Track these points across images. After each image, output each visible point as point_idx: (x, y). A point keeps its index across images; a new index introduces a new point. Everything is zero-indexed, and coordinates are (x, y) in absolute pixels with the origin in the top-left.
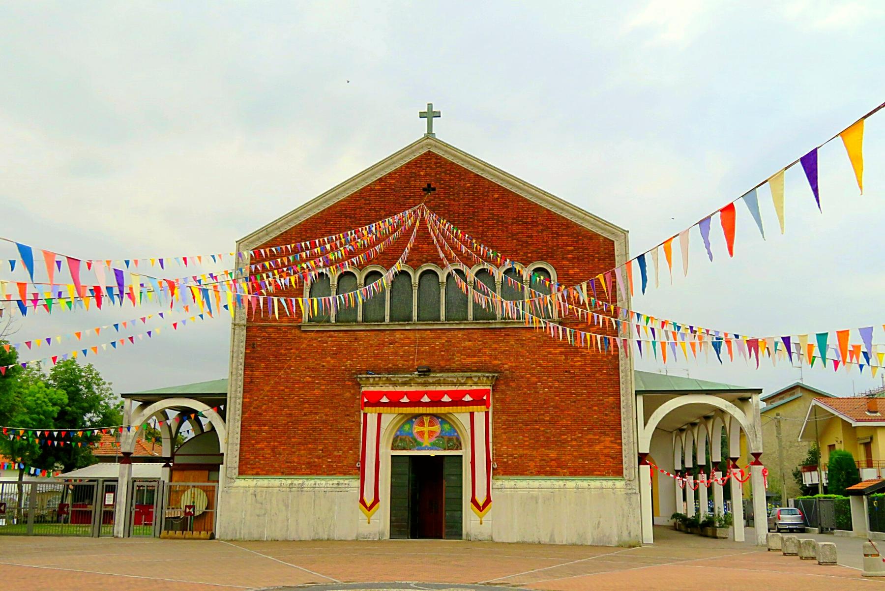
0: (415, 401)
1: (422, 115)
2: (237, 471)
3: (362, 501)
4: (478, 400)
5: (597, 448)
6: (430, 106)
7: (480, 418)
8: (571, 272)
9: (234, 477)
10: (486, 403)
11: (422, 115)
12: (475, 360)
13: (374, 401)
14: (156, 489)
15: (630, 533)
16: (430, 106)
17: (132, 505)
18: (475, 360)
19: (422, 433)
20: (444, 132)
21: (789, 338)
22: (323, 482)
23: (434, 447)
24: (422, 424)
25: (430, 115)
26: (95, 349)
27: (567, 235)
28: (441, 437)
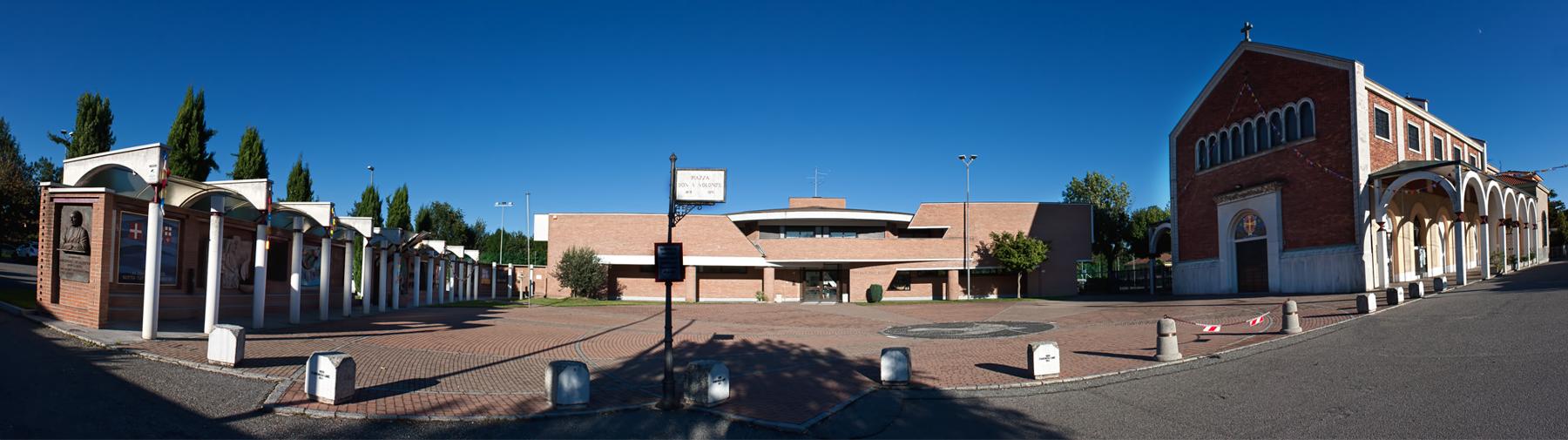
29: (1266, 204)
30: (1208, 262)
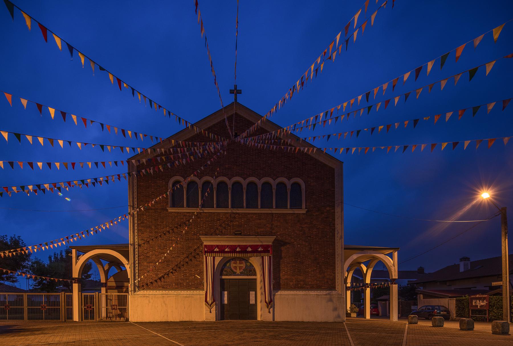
0: (233, 249)
1: (232, 92)
3: (206, 301)
4: (266, 249)
6: (236, 87)
7: (266, 259)
10: (268, 252)
11: (232, 92)
13: (210, 250)
14: (83, 319)
16: (236, 87)
17: (82, 305)
19: (236, 268)
20: (241, 99)
21: (230, 90)
23: (242, 274)
24: (236, 263)
25: (236, 91)
26: (103, 163)
28: (245, 270)
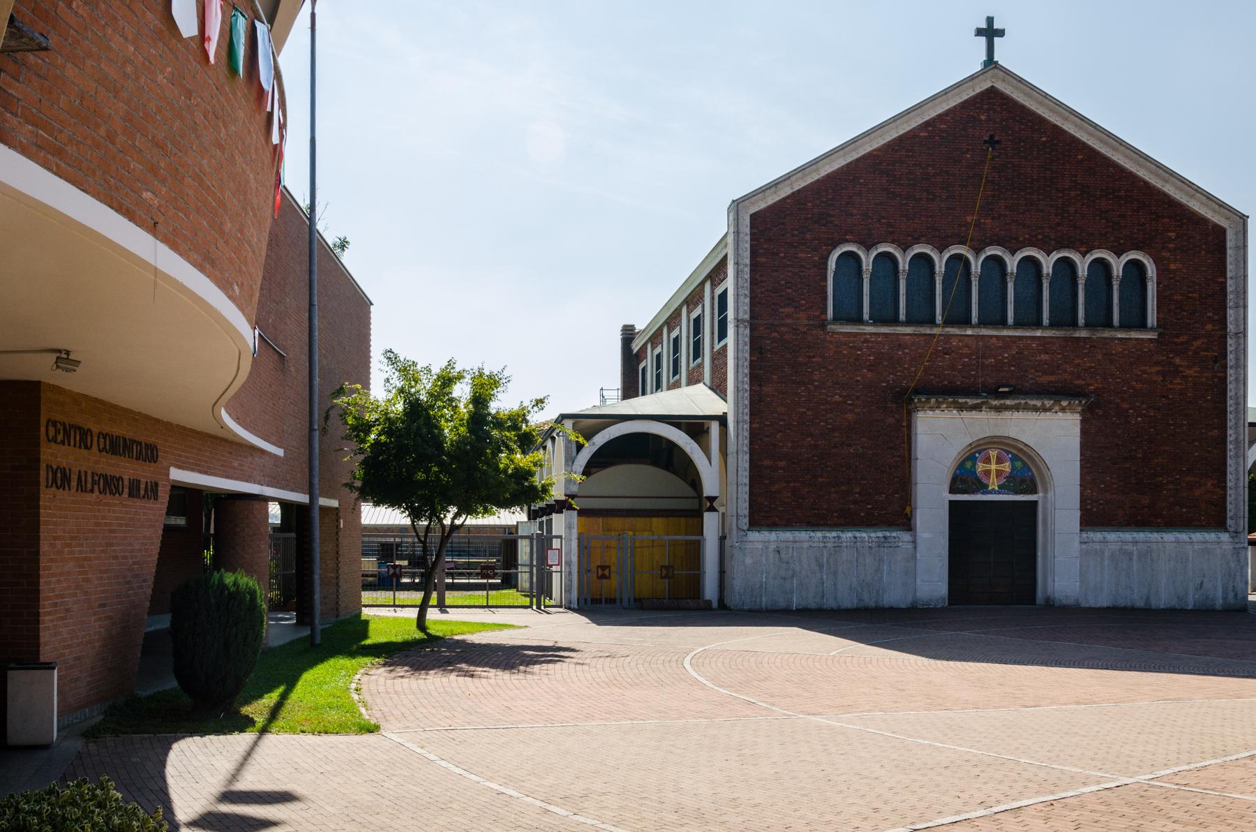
2: (746, 520)
5: (1197, 492)
8: (1172, 267)
9: (745, 528)
12: (1052, 378)
15: (1236, 595)
18: (1052, 378)
22: (864, 535)
27: (1169, 217)
29: (1054, 436)
30: (868, 536)
